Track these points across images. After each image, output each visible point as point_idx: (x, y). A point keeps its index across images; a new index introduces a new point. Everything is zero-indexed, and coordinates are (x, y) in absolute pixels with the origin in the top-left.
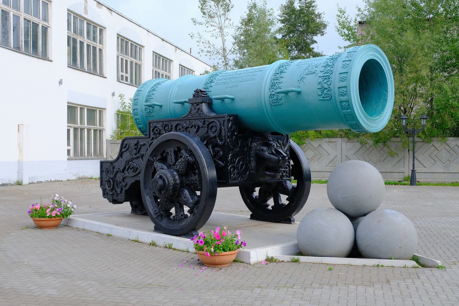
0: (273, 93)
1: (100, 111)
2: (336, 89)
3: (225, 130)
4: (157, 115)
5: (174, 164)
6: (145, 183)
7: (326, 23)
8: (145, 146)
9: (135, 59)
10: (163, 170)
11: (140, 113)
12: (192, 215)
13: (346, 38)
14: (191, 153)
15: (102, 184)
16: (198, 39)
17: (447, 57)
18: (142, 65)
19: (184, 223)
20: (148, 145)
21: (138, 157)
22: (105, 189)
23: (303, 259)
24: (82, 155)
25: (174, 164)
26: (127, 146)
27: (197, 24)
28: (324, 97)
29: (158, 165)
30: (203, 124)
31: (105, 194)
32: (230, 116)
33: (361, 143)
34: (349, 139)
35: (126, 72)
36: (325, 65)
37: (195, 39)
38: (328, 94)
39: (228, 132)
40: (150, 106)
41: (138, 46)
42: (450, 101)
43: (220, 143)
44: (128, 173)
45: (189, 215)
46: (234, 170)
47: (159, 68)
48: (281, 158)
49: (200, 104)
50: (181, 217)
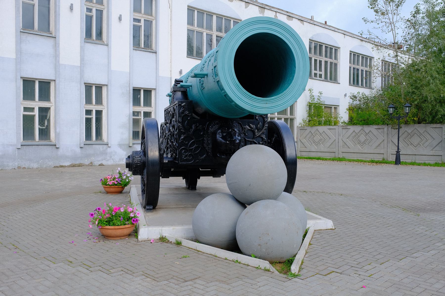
35: (320, 70)
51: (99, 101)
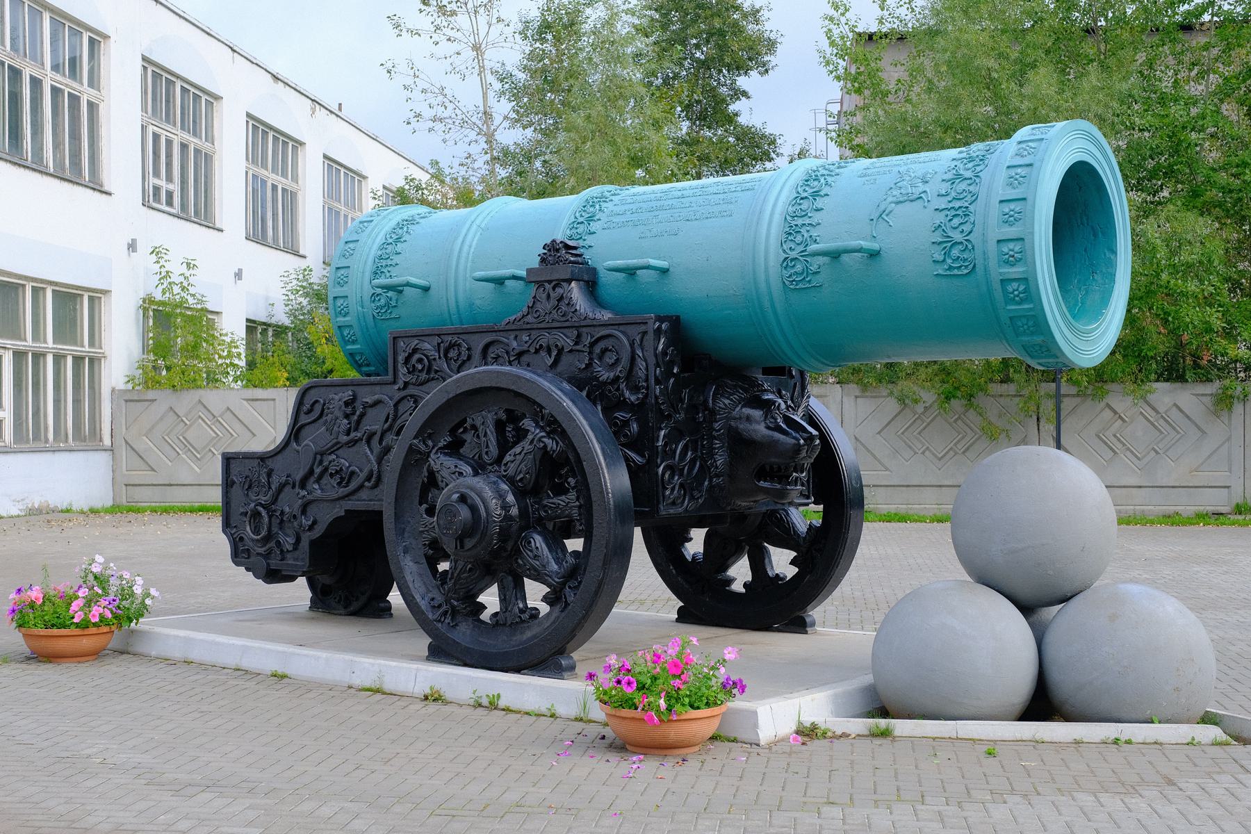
0: (793, 254)
1: (91, 299)
2: (992, 247)
3: (646, 361)
4: (411, 315)
5: (499, 461)
6: (398, 517)
7: (773, 36)
8: (379, 407)
9: (195, 134)
10: (461, 479)
11: (355, 308)
12: (558, 608)
13: (849, 85)
14: (555, 427)
15: (227, 525)
16: (409, 81)
17: (1152, 149)
18: (216, 157)
19: (528, 634)
20: (392, 403)
21: (355, 442)
22: (241, 539)
23: (902, 727)
24: (36, 437)
25: (499, 461)
26: (318, 408)
27: (404, 33)
28: (950, 268)
29: (442, 463)
30: (576, 343)
31: (240, 554)
32: (661, 319)
33: (901, 400)
34: (865, 387)
35: (169, 179)
36: (949, 176)
37: (400, 80)
38: (965, 260)
39: (657, 365)
40: (388, 288)
41: (204, 97)
42: (1164, 276)
43: (633, 398)
44: (322, 490)
45: (544, 609)
46: (672, 476)
47: (264, 166)
48: (802, 442)
49: (564, 284)
50: (515, 615)
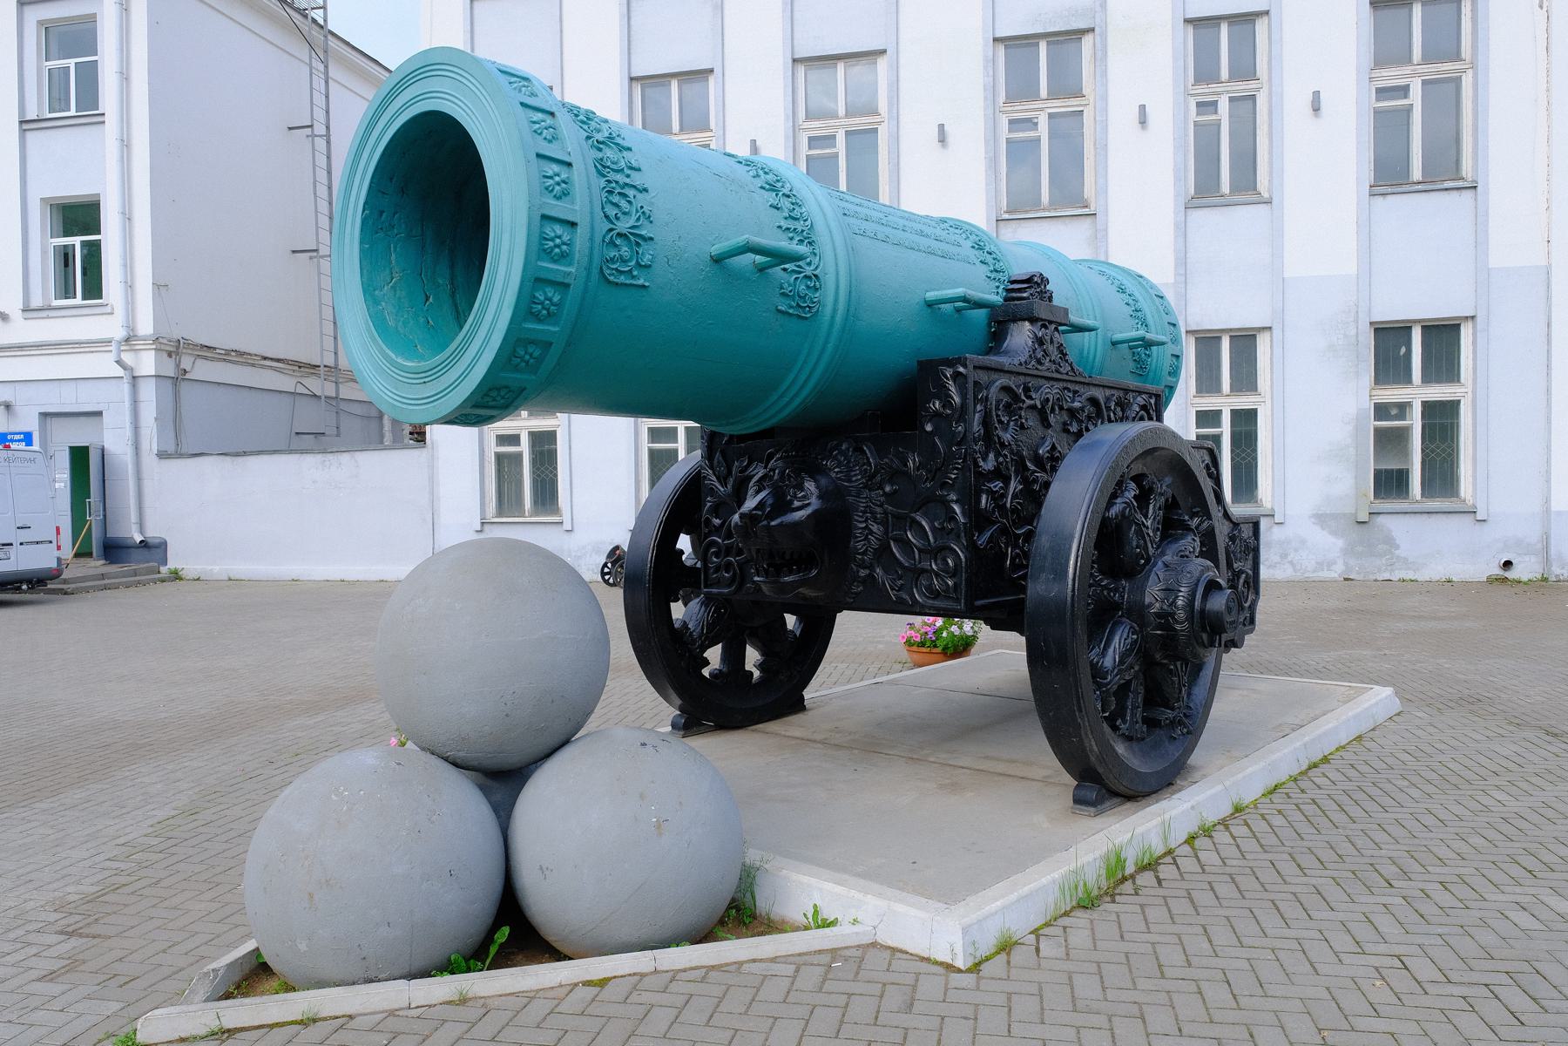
51: (1246, 379)
